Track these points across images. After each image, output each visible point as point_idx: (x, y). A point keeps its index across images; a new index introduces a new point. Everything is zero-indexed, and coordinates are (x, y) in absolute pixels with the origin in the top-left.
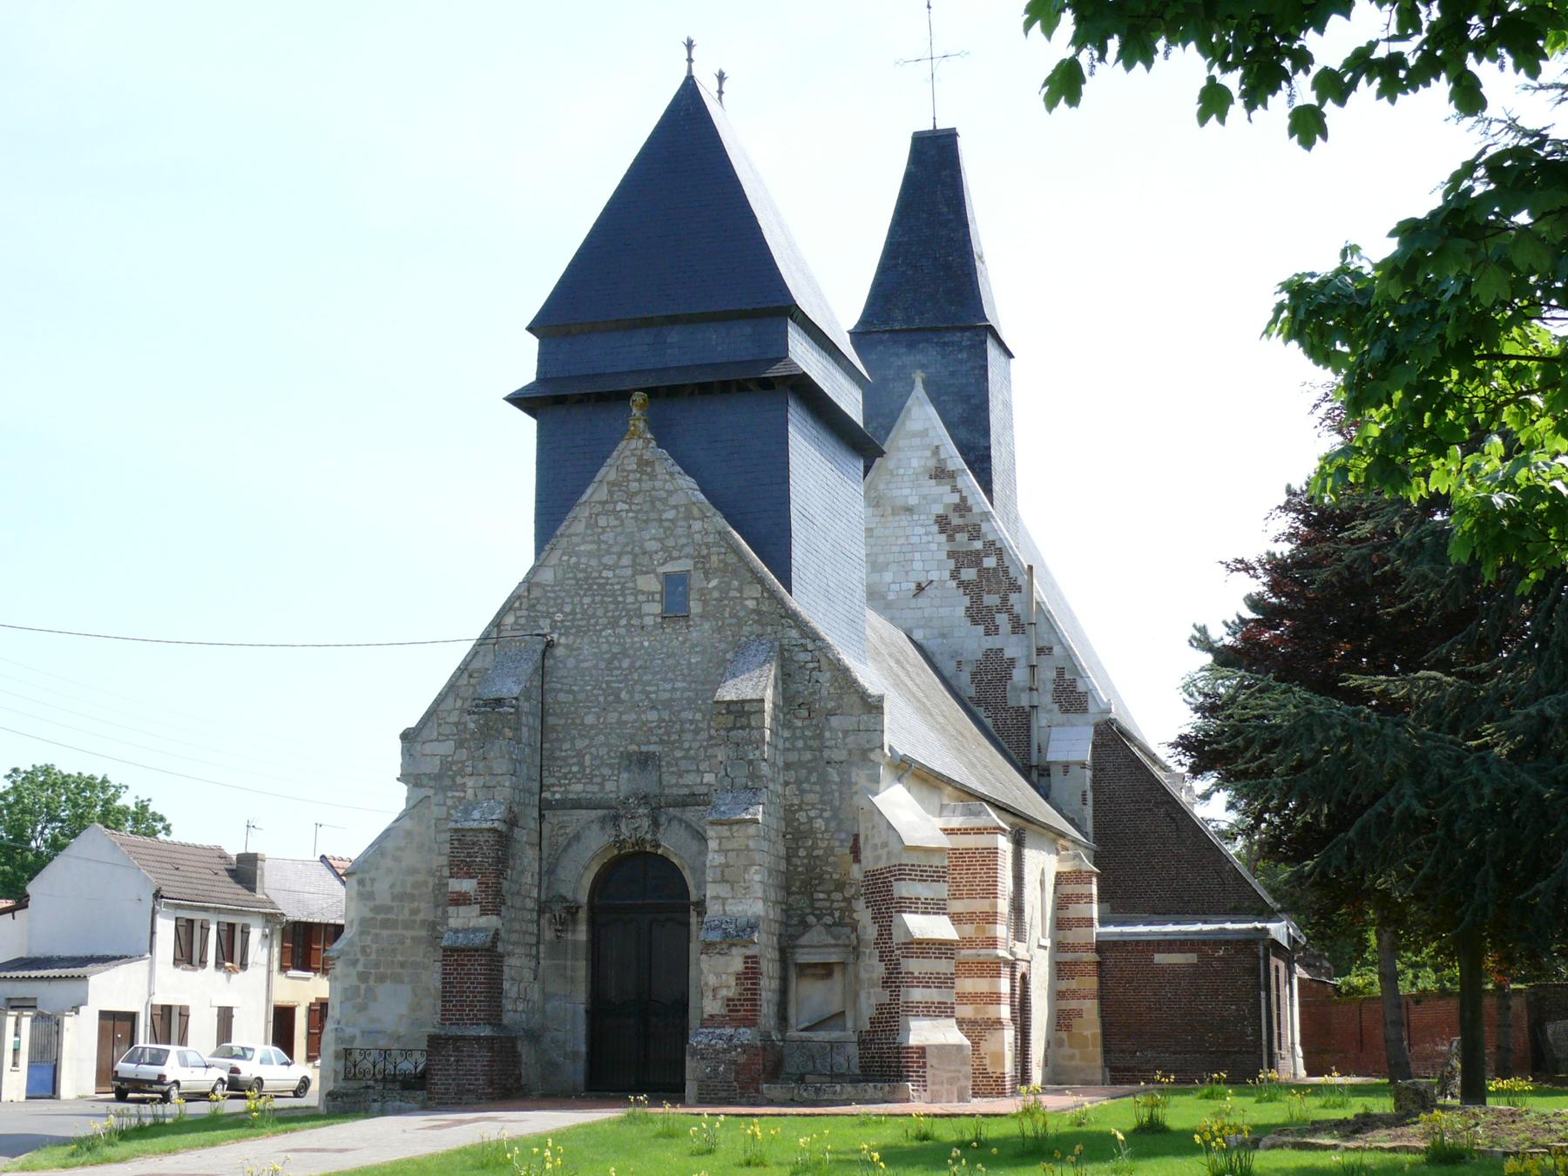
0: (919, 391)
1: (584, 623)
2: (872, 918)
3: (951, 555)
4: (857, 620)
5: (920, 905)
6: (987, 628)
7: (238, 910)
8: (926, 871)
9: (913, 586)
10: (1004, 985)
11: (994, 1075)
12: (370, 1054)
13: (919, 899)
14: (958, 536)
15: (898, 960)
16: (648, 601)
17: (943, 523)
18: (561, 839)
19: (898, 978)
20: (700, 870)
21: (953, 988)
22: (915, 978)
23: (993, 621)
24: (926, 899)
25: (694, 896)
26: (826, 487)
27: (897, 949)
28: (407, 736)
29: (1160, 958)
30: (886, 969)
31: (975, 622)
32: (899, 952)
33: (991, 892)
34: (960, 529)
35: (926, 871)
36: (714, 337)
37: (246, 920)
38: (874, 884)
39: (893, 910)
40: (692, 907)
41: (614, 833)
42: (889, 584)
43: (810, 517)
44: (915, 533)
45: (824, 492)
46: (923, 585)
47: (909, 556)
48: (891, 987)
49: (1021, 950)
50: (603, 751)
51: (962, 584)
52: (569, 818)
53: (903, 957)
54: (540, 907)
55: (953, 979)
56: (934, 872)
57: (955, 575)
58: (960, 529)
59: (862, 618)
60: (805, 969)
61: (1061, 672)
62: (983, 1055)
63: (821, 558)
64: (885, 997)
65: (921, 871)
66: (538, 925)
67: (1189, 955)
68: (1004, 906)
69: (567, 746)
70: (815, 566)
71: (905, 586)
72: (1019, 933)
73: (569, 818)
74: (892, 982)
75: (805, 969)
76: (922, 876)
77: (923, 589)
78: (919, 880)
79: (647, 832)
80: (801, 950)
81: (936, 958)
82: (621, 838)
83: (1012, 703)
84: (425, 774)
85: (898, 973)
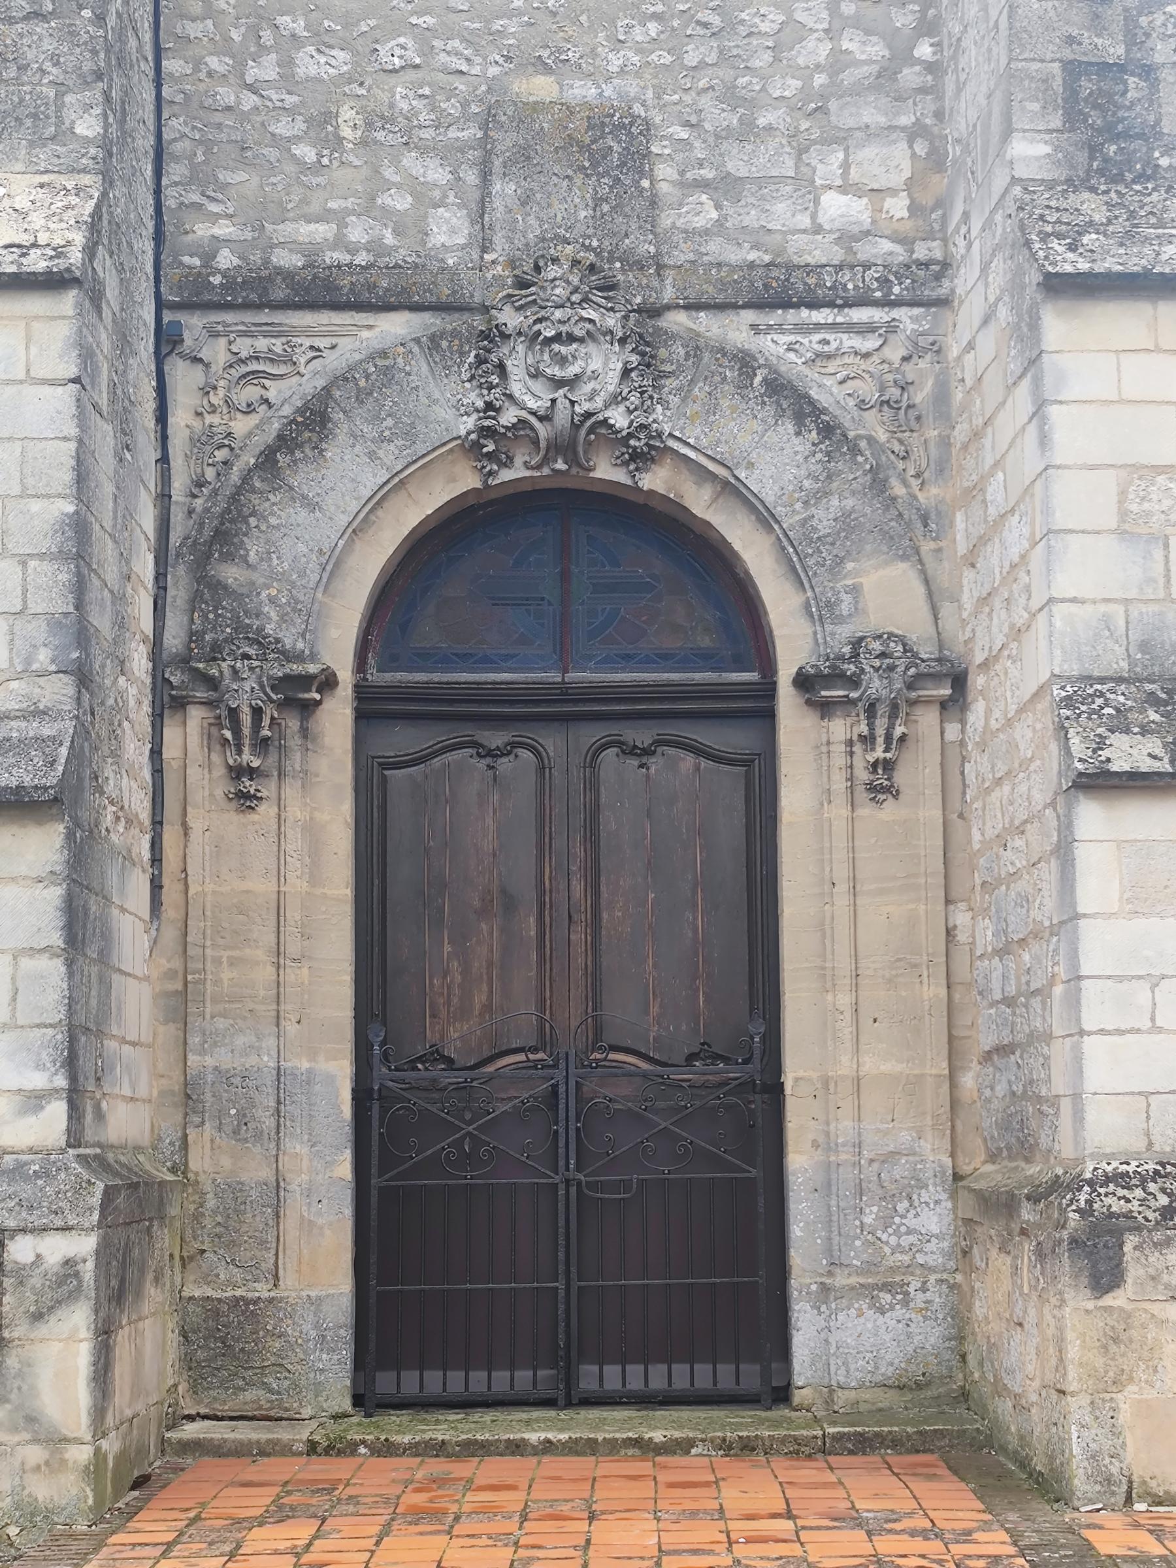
18: (241, 425)
69: (265, 70)
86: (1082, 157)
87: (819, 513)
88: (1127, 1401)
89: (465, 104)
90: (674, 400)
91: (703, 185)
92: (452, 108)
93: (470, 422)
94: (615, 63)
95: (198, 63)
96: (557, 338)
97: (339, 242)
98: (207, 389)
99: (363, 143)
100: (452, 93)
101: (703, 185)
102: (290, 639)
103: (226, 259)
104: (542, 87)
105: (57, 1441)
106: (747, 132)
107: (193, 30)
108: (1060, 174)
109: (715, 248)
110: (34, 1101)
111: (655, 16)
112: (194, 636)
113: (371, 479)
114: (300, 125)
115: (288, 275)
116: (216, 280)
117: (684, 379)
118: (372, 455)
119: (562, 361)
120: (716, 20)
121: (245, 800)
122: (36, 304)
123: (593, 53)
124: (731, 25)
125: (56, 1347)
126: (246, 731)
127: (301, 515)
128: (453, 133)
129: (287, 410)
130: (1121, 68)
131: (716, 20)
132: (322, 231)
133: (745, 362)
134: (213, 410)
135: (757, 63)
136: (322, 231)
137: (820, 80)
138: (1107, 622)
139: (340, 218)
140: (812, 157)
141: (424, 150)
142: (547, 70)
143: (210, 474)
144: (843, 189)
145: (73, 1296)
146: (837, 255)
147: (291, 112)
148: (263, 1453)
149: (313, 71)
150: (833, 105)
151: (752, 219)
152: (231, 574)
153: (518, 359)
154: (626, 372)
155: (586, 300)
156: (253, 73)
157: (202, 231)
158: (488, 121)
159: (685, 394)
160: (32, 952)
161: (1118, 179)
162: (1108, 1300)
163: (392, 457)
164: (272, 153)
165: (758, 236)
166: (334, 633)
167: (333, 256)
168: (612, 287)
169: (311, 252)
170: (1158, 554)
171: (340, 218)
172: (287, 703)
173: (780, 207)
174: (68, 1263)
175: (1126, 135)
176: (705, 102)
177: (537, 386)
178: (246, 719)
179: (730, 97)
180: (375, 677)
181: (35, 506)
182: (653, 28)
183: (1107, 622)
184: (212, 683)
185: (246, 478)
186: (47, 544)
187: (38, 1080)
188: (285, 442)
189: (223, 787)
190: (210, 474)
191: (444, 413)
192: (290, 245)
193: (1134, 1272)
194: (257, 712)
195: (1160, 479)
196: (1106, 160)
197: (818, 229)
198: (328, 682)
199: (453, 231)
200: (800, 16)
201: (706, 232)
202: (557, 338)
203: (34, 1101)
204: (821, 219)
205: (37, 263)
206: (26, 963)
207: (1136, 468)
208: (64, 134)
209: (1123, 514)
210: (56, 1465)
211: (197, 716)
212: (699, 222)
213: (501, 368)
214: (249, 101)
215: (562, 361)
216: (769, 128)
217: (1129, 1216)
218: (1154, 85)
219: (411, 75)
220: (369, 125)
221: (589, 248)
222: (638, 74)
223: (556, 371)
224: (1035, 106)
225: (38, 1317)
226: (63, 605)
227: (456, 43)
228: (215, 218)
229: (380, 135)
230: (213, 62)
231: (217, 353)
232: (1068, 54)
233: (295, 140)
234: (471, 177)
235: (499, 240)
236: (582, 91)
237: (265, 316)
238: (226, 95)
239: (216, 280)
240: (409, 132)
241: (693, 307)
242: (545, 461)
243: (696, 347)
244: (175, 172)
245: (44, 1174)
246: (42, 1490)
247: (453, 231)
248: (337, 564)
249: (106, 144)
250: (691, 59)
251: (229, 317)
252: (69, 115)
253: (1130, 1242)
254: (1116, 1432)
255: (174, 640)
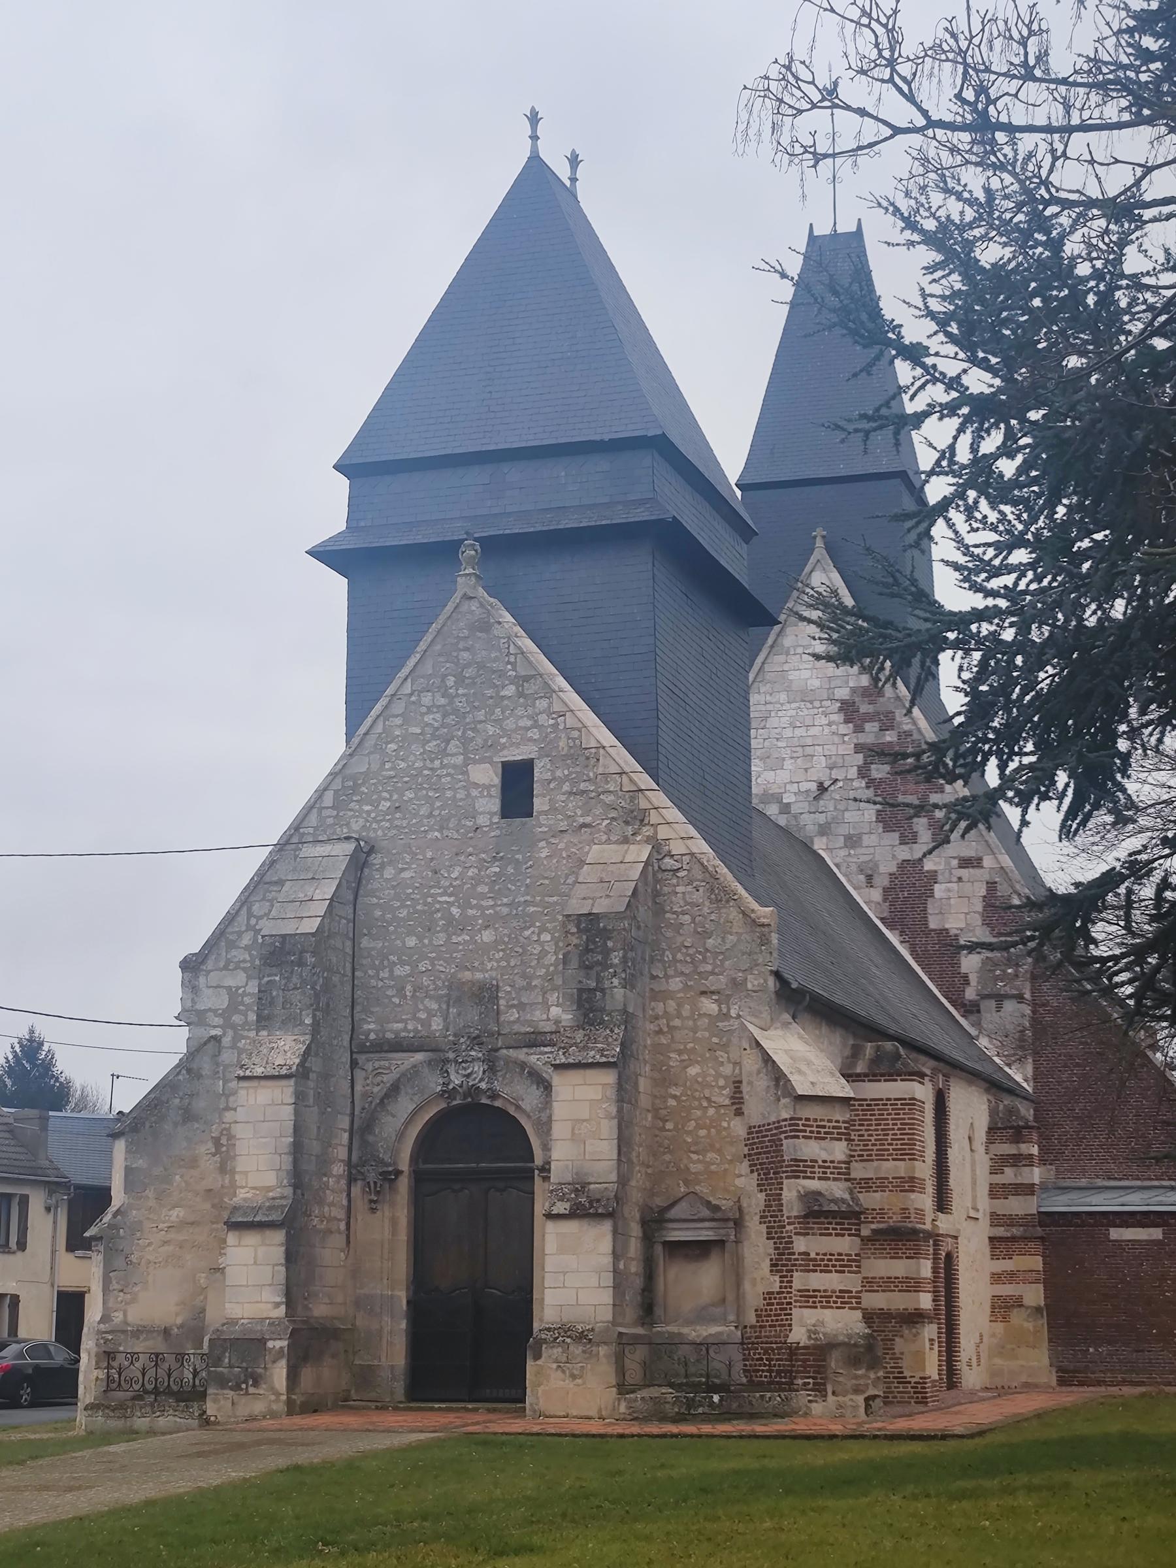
0: (819, 552)
1: (405, 823)
2: (758, 1185)
3: (859, 748)
4: (741, 822)
5: (817, 1170)
6: (902, 836)
7: (35, 1180)
8: (824, 1127)
9: (813, 786)
10: (925, 1269)
11: (913, 1380)
12: (138, 1359)
13: (816, 1161)
14: (868, 726)
15: (790, 1237)
16: (482, 796)
17: (848, 710)
18: (376, 1089)
19: (790, 1260)
20: (545, 1127)
21: (864, 1278)
22: (811, 1260)
23: (910, 827)
24: (825, 1161)
25: (538, 1161)
26: (702, 660)
27: (789, 1224)
28: (190, 965)
29: (1115, 1234)
30: (776, 1249)
31: (888, 828)
32: (791, 1227)
33: (908, 1153)
34: (868, 718)
35: (824, 1127)
36: (563, 474)
37: (25, 1191)
38: (760, 1142)
39: (784, 1175)
40: (536, 1172)
41: (441, 1081)
42: (785, 784)
43: (681, 695)
44: (800, 643)
45: (700, 665)
46: (826, 784)
47: (809, 750)
48: (782, 1271)
49: (944, 1224)
50: (425, 981)
51: (871, 783)
52: (386, 1064)
53: (796, 1234)
54: (350, 1173)
55: (859, 1261)
56: (834, 1127)
57: (863, 772)
58: (868, 718)
59: (747, 819)
60: (678, 1249)
61: (991, 886)
62: (898, 1355)
63: (695, 745)
64: (775, 1283)
65: (818, 1126)
66: (349, 1195)
67: (1152, 1230)
68: (925, 1169)
69: (384, 974)
70: (688, 755)
71: (804, 786)
72: (942, 1203)
73: (386, 1064)
74: (783, 1265)
75: (678, 1249)
76: (819, 1132)
77: (826, 789)
78: (816, 1138)
79: (482, 1080)
80: (671, 1225)
81: (837, 1235)
82: (451, 1087)
83: (933, 924)
84: (210, 1010)
85: (789, 1254)
86: (582, 1018)
87: (543, 1115)
88: (540, 1390)
89: (444, 983)
90: (500, 1079)
91: (513, 1006)
92: (440, 983)
93: (439, 1088)
94: (489, 966)
95: (366, 973)
96: (463, 1062)
97: (405, 1029)
98: (366, 1078)
99: (412, 996)
100: (440, 979)
101: (513, 1006)
102: (387, 1159)
103: (372, 1036)
104: (467, 975)
105: (278, 1394)
106: (529, 987)
107: (364, 962)
108: (576, 1024)
109: (516, 1028)
110: (277, 1305)
111: (502, 950)
112: (360, 1158)
113: (411, 1107)
114: (395, 991)
115: (388, 1041)
116: (368, 1044)
117: (504, 1071)
118: (411, 1099)
119: (465, 1069)
120: (521, 950)
121: (373, 1210)
122: (284, 1082)
123: (483, 963)
124: (525, 952)
125: (278, 1370)
126: (372, 1188)
127: (390, 1118)
128: (440, 992)
129: (388, 1085)
130: (595, 990)
131: (521, 950)
132: (400, 1026)
133: (523, 1065)
134: (368, 1085)
135: (532, 964)
136: (400, 1026)
137: (552, 968)
138: (567, 1166)
139: (405, 1021)
140: (548, 996)
141: (431, 997)
142: (469, 970)
143: (367, 1106)
144: (557, 1006)
145: (282, 1357)
146: (554, 1028)
147: (392, 987)
148: (364, 1409)
149: (399, 973)
150: (555, 977)
151: (528, 1017)
152: (371, 1138)
153: (452, 1069)
154: (484, 1072)
155: (472, 1048)
156: (382, 975)
157: (366, 1027)
158: (450, 988)
159: (504, 1077)
160: (277, 1265)
161: (592, 1025)
162: (537, 1362)
163: (418, 1099)
164: (386, 1001)
165: (529, 1023)
166: (402, 1155)
167: (403, 1034)
168: (482, 1044)
169: (397, 1033)
170: (582, 1146)
171: (405, 1021)
172: (385, 1179)
173: (538, 1013)
174: (281, 1348)
175: (595, 1011)
176: (516, 978)
177: (459, 1076)
178: (372, 1185)
179: (524, 976)
180: (421, 1166)
181: (283, 1139)
182: (501, 954)
183: (567, 1166)
184: (362, 1174)
185: (375, 1108)
186: (286, 1150)
187: (278, 1299)
188: (387, 1096)
189: (367, 1206)
190: (367, 1106)
191: (432, 1085)
192: (391, 1031)
193: (544, 1355)
194: (375, 1183)
195: (585, 1123)
196: (589, 1018)
197: (548, 1019)
198: (398, 1173)
199: (438, 1025)
200: (546, 948)
201: (514, 1022)
202: (463, 1062)
203: (277, 1305)
204: (550, 1016)
205: (284, 1072)
206: (276, 1268)
207: (577, 1120)
208: (302, 1023)
209: (573, 1134)
210: (277, 1400)
211: (359, 1183)
212: (512, 1019)
213: (447, 1072)
214: (380, 984)
215: (465, 1069)
216: (536, 986)
217: (545, 1339)
218: (604, 995)
219: (429, 973)
220: (415, 991)
221: (477, 1029)
222: (496, 970)
223: (464, 1072)
224: (568, 1003)
225: (274, 1362)
226: (290, 1167)
227: (441, 962)
228: (369, 1023)
229: (418, 994)
230: (370, 972)
231: (369, 1066)
232: (579, 986)
233: (393, 996)
234: (444, 1006)
235: (451, 1027)
236: (479, 976)
237: (383, 1055)
238: (373, 982)
239: (368, 1044)
240: (427, 992)
241: (508, 1048)
242: (464, 1099)
243: (508, 1061)
244: (358, 1008)
245: (278, 1325)
246: (274, 1407)
247: (438, 1025)
248: (402, 1134)
249: (312, 1025)
250: (512, 964)
251: (372, 1055)
252: (303, 1018)
253: (544, 1346)
254: (538, 1398)
255: (355, 1158)
